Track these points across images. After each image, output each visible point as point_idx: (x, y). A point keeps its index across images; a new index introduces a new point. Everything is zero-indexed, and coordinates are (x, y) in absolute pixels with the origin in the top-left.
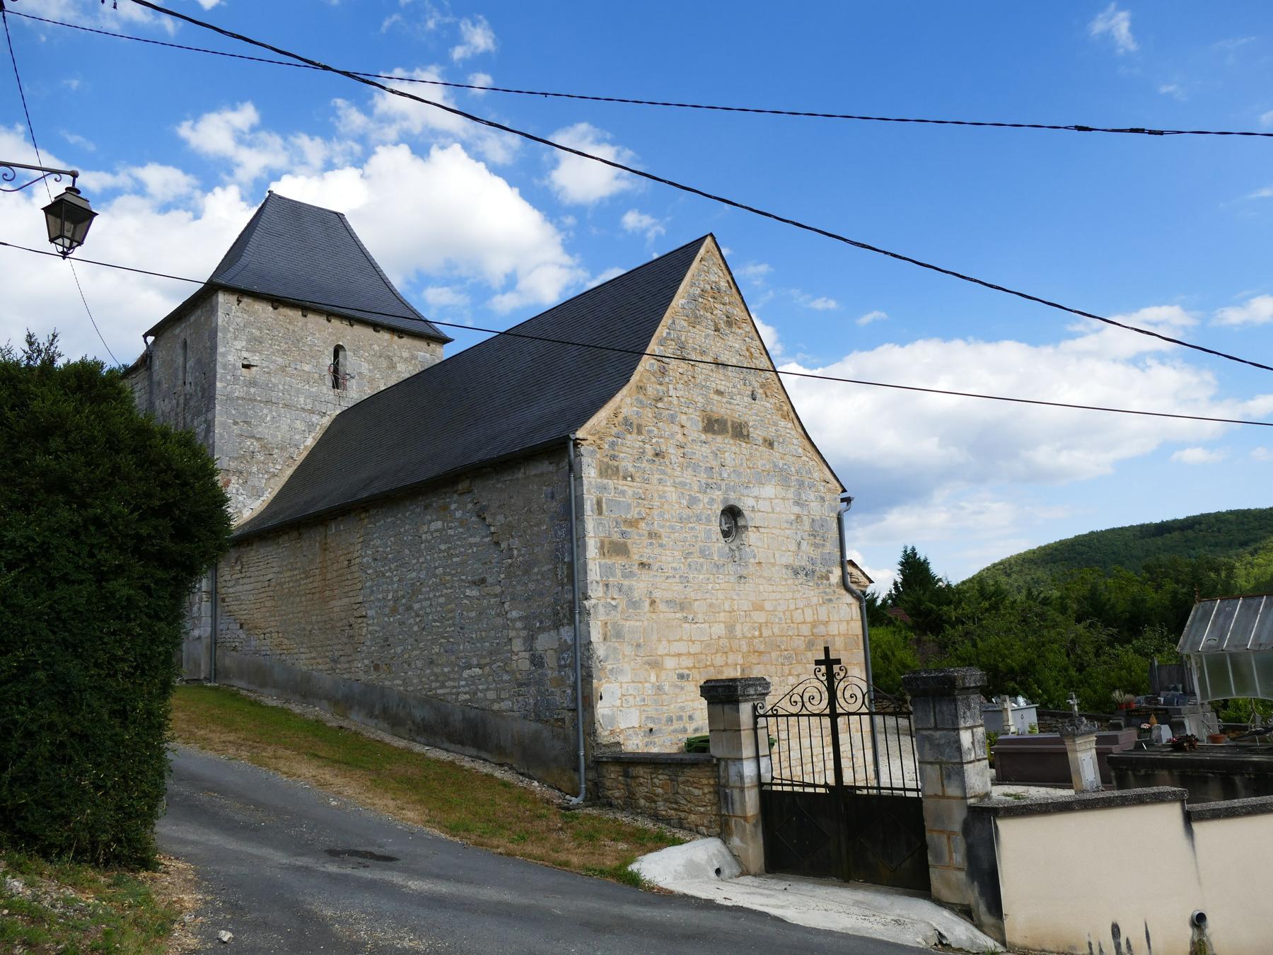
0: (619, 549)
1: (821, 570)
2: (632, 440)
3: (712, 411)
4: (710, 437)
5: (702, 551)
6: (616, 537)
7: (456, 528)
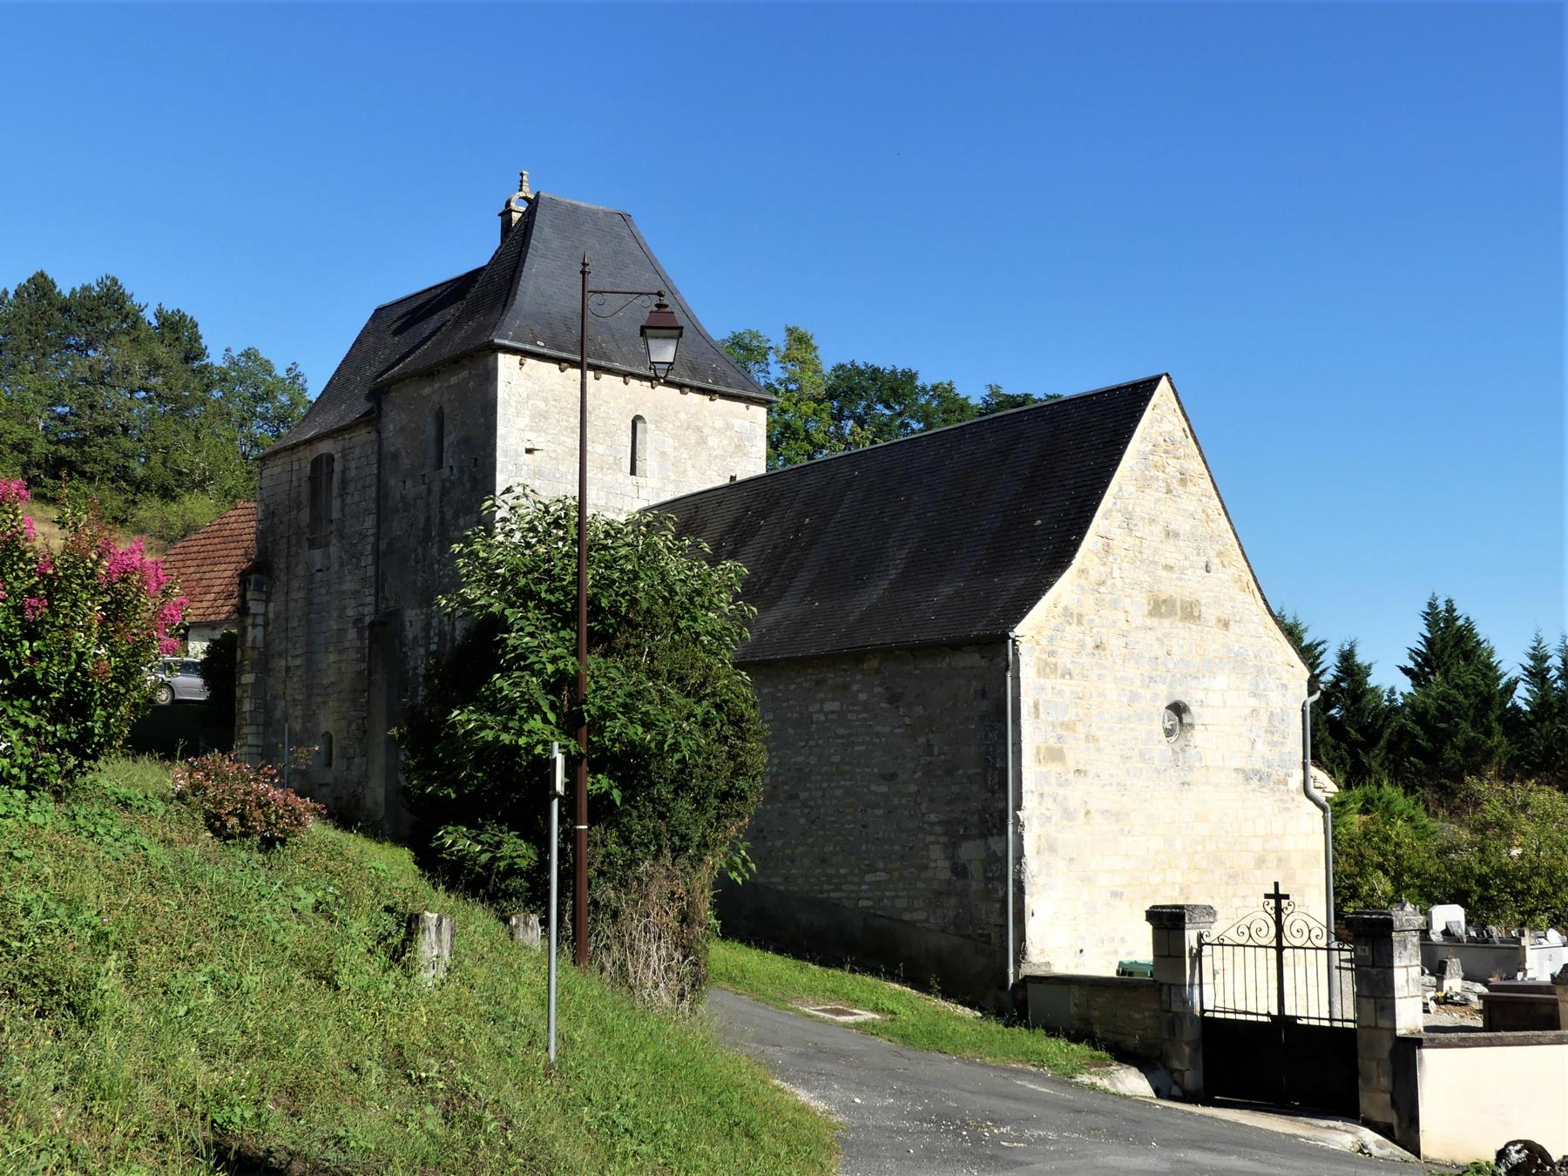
0: (1056, 755)
1: (1278, 773)
2: (1072, 630)
3: (1159, 591)
4: (1154, 622)
5: (1142, 755)
6: (1052, 742)
7: (858, 712)
